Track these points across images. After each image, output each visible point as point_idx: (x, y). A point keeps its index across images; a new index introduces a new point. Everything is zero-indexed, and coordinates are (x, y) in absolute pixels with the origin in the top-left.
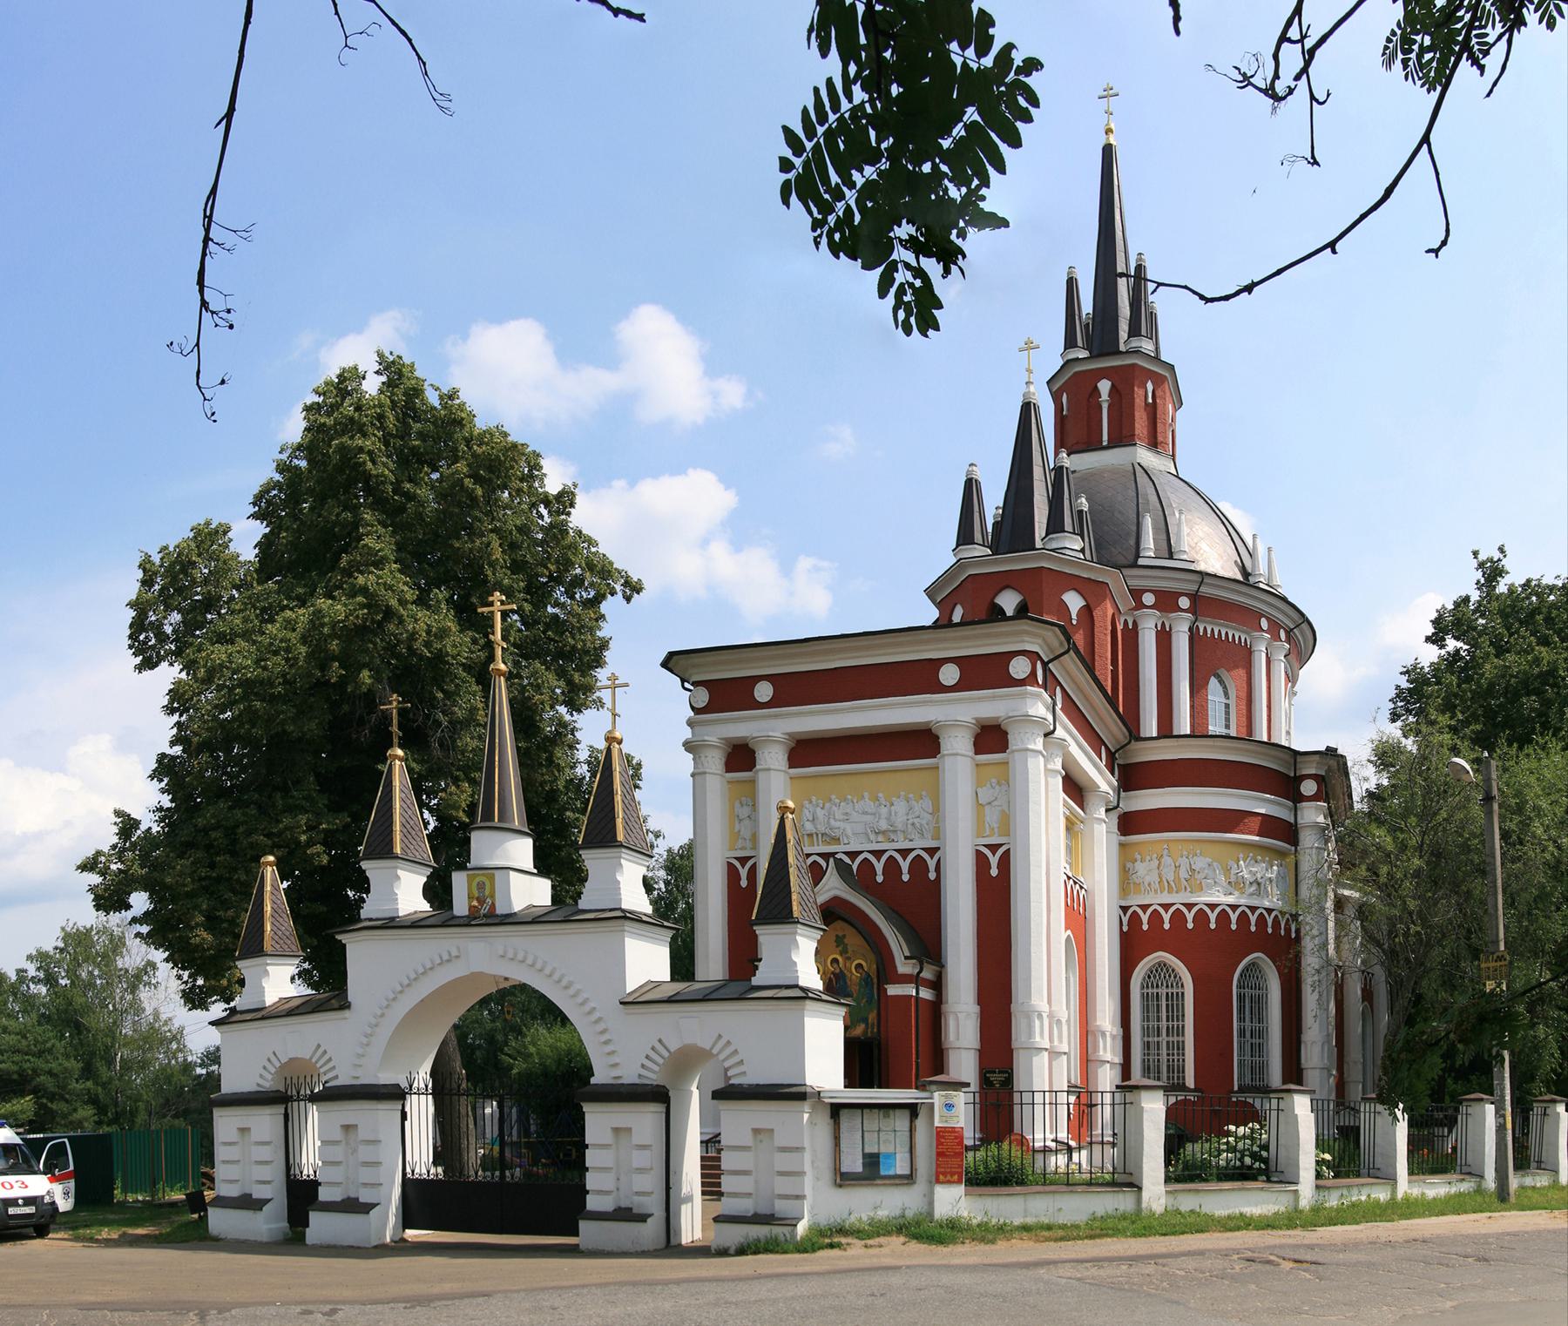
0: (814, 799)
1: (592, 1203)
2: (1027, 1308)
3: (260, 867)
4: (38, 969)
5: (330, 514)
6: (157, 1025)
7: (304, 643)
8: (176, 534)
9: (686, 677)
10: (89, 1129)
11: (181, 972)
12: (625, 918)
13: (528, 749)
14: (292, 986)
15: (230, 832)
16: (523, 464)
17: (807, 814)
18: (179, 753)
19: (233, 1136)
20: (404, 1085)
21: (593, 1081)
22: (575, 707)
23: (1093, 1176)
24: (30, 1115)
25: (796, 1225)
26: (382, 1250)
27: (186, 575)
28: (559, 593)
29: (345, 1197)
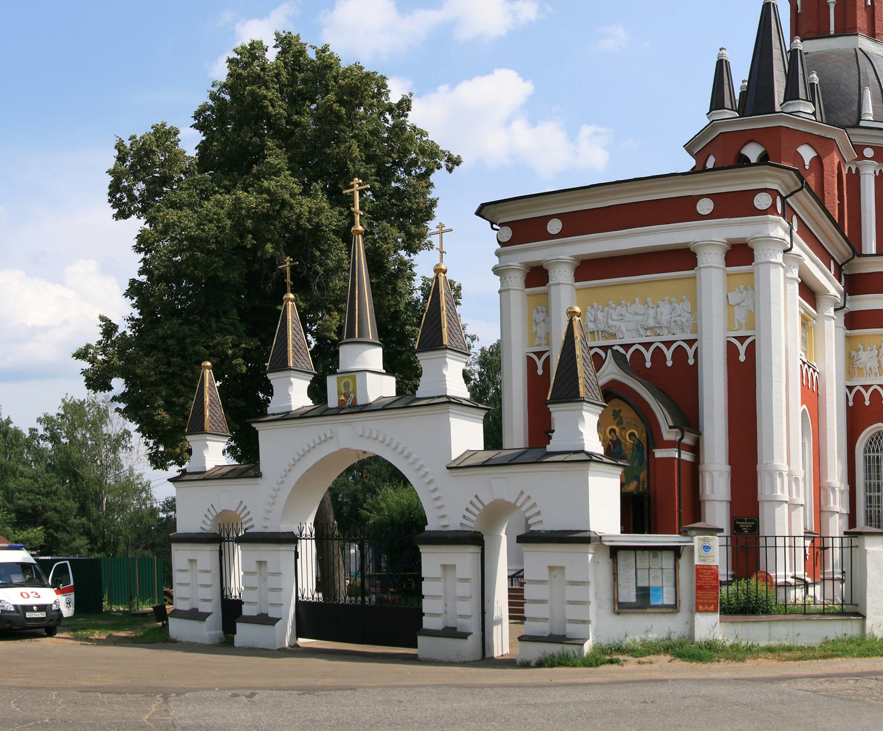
0: (595, 304)
1: (428, 623)
2: (772, 714)
3: (201, 369)
4: (46, 429)
5: (246, 136)
6: (132, 479)
7: (229, 218)
8: (142, 129)
9: (495, 220)
10: (84, 554)
11: (148, 440)
12: (450, 402)
13: (378, 283)
14: (224, 457)
15: (181, 341)
16: (373, 86)
17: (590, 317)
18: (145, 280)
19: (185, 565)
20: (297, 532)
21: (427, 528)
22: (412, 249)
23: (826, 607)
24: (41, 541)
25: (583, 645)
26: (282, 652)
27: (149, 158)
28: (400, 173)
29: (260, 613)
